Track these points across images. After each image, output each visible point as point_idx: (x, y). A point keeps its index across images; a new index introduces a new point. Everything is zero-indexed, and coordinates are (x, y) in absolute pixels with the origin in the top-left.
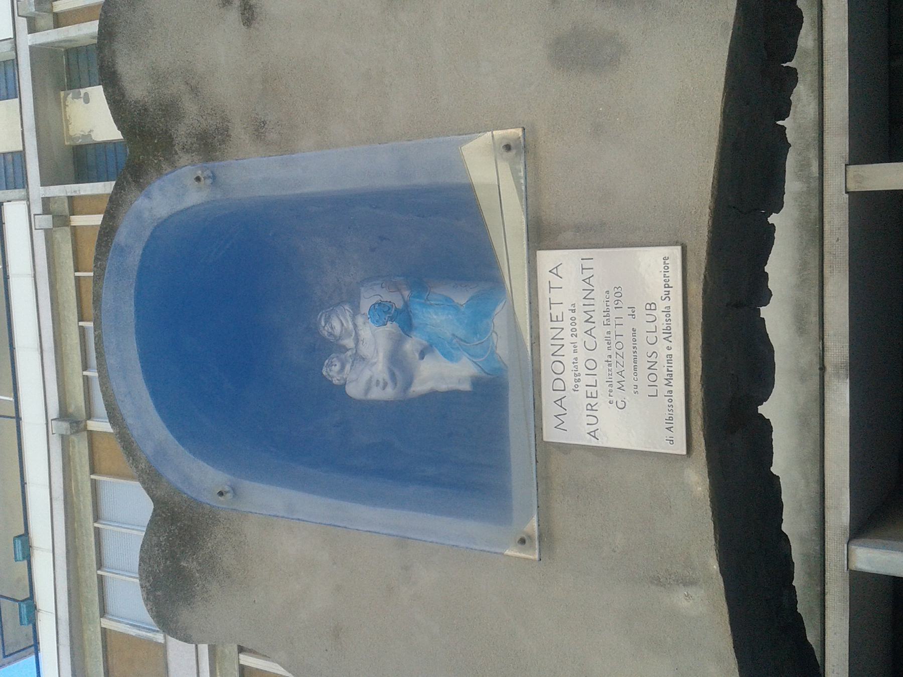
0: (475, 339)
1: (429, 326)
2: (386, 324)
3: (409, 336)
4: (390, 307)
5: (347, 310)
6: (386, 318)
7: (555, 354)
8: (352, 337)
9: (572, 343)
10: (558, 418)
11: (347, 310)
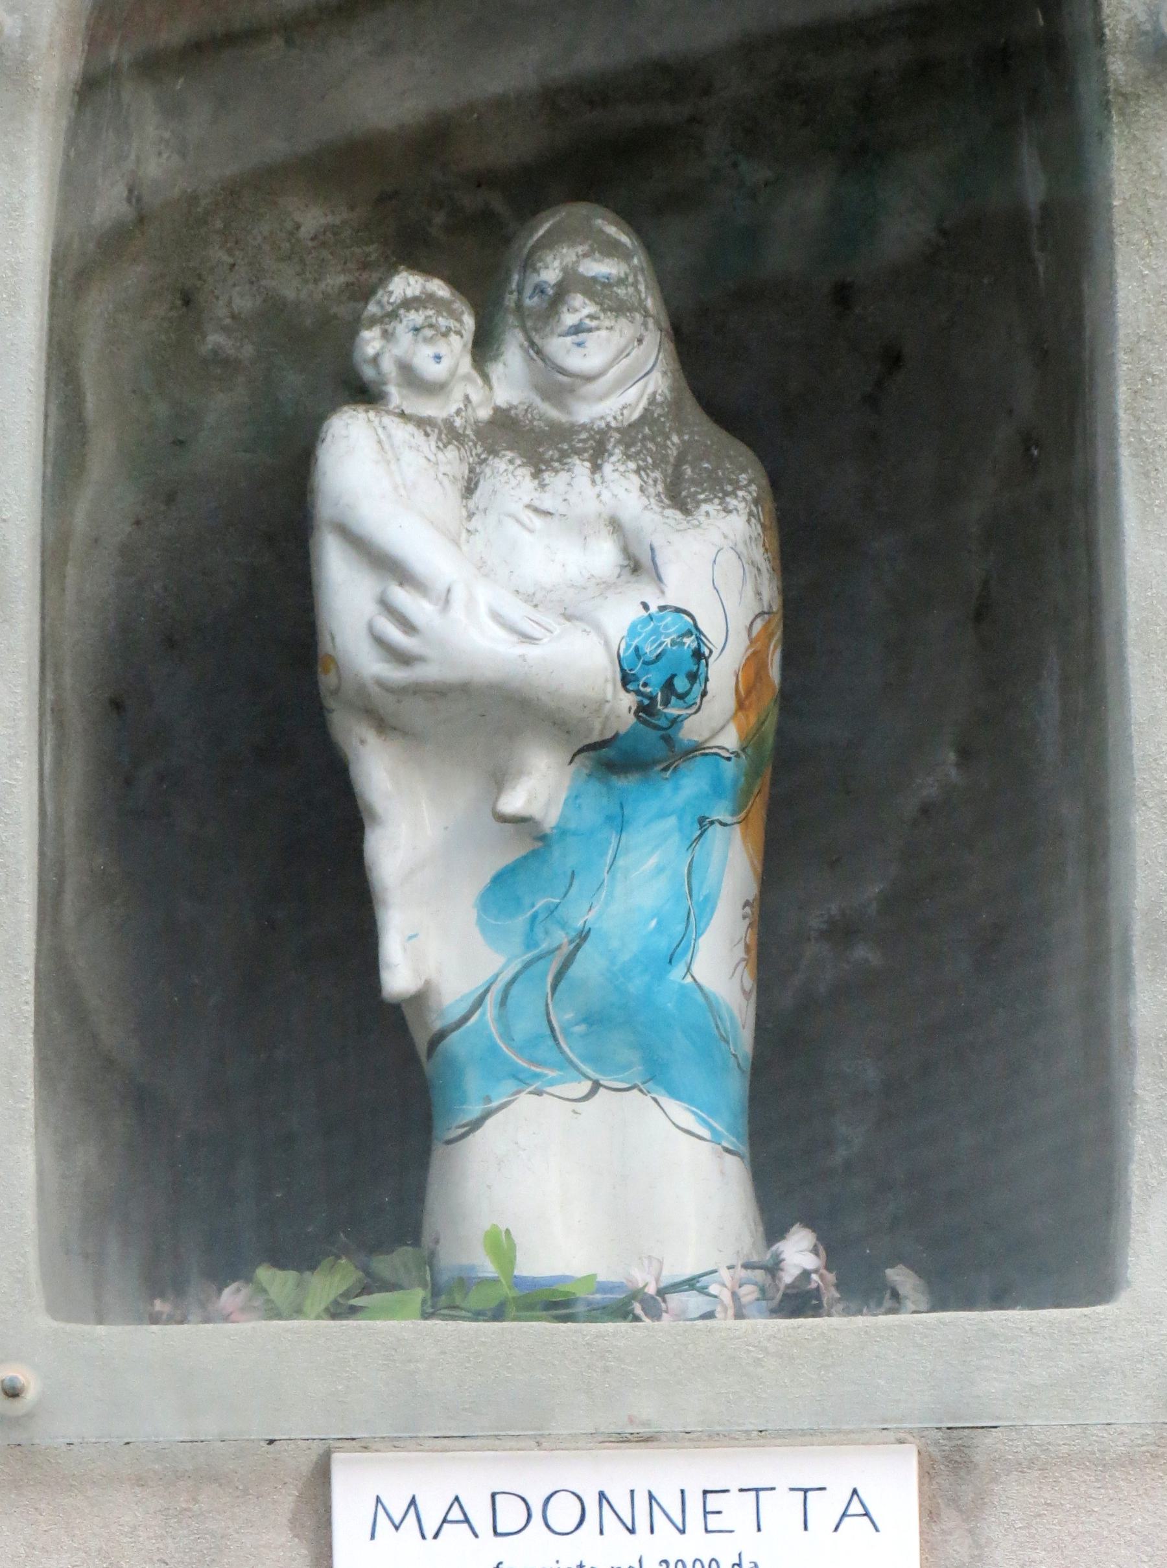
0: (569, 1016)
1: (614, 841)
2: (628, 691)
3: (575, 755)
4: (689, 699)
5: (646, 386)
6: (648, 690)
7: (604, 1502)
8: (537, 401)
9: (640, 1561)
10: (377, 1507)
11: (646, 386)
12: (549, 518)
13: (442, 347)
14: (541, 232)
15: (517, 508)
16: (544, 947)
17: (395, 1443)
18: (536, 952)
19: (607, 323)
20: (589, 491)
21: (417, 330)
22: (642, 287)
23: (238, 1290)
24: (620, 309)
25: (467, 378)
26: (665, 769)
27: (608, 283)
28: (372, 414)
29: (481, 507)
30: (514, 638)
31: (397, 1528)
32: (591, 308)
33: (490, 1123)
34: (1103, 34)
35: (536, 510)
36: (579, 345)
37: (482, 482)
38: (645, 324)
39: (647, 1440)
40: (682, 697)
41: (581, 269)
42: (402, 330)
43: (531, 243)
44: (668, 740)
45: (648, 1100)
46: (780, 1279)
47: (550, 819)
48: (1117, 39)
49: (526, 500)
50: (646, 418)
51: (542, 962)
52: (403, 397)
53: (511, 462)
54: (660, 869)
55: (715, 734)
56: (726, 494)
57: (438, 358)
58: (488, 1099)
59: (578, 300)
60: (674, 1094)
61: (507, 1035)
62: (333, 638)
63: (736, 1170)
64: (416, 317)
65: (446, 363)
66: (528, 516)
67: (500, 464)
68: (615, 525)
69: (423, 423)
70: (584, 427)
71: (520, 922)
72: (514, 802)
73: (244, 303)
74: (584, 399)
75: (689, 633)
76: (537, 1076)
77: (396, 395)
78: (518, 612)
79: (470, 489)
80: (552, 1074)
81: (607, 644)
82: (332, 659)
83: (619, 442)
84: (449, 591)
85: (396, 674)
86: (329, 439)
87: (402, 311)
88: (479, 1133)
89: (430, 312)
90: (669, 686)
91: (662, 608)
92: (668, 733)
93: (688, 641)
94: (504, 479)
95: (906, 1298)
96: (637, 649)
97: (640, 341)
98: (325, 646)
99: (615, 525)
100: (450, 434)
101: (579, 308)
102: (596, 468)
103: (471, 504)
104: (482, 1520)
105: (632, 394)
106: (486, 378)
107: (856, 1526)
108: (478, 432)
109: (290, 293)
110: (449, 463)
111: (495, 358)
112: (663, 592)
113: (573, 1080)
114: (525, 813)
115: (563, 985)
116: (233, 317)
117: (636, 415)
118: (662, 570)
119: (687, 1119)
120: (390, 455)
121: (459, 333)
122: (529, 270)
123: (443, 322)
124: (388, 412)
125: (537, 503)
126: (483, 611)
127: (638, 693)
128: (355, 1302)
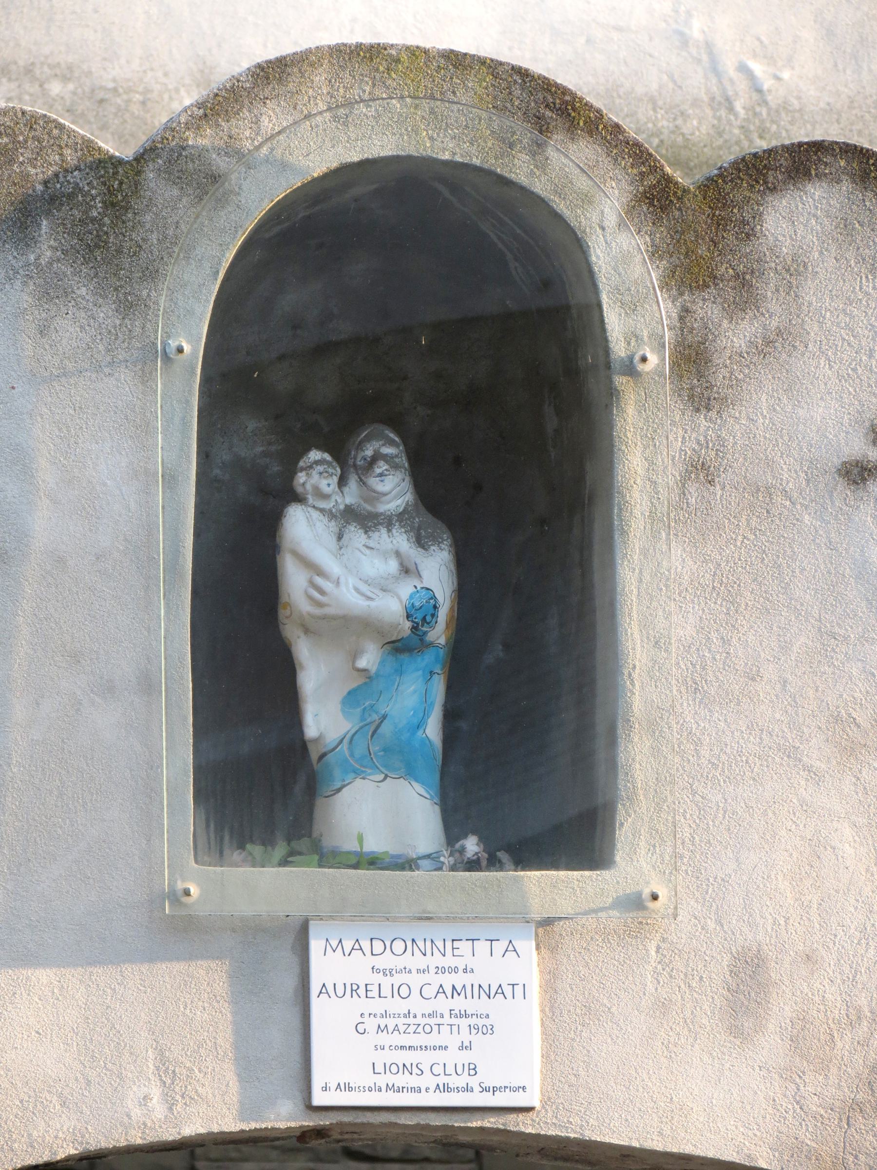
0: (377, 748)
1: (398, 679)
6: (416, 620)
12: (372, 550)
13: (330, 481)
14: (364, 435)
15: (360, 546)
16: (369, 720)
17: (332, 918)
18: (365, 723)
19: (392, 473)
20: (388, 540)
21: (321, 473)
22: (404, 458)
23: (241, 853)
24: (396, 467)
25: (337, 493)
26: (419, 651)
27: (392, 457)
28: (303, 506)
29: (345, 544)
30: (364, 598)
31: (334, 951)
32: (386, 467)
33: (344, 790)
34: (610, 366)
35: (368, 547)
36: (382, 481)
37: (345, 535)
38: (405, 473)
39: (429, 919)
40: (428, 623)
41: (381, 451)
42: (315, 473)
43: (359, 439)
44: (421, 640)
45: (407, 782)
46: (465, 856)
47: (373, 669)
48: (616, 368)
49: (363, 543)
50: (405, 511)
51: (367, 727)
52: (314, 500)
53: (355, 527)
54: (415, 692)
55: (438, 638)
56: (440, 543)
57: (329, 485)
58: (344, 780)
59: (381, 463)
60: (416, 780)
61: (352, 755)
62: (289, 596)
63: (437, 809)
64: (320, 468)
65: (332, 487)
66: (364, 549)
67: (352, 528)
68: (398, 554)
69: (322, 510)
70: (381, 514)
71: (359, 710)
72: (362, 663)
73: (227, 457)
74: (381, 502)
75: (432, 598)
76: (363, 772)
77: (311, 500)
78: (364, 588)
79: (340, 537)
80: (369, 771)
81: (401, 601)
82: (287, 605)
83: (397, 520)
84: (339, 578)
85: (317, 611)
86: (288, 516)
87: (314, 466)
88: (340, 793)
89: (326, 466)
90: (424, 619)
91: (422, 588)
92: (422, 637)
93: (431, 601)
94: (354, 534)
95: (505, 864)
96: (413, 604)
97: (404, 481)
98: (284, 599)
99: (398, 554)
100: (331, 515)
101: (382, 467)
102: (389, 531)
103: (341, 544)
104: (367, 950)
105: (399, 502)
106: (342, 492)
107: (511, 955)
108: (341, 514)
109: (243, 455)
110: (333, 527)
111: (345, 485)
112: (422, 582)
113: (377, 774)
114: (366, 668)
115: (375, 736)
116: (223, 463)
117: (401, 510)
118: (421, 573)
119: (422, 791)
120: (311, 524)
121: (336, 475)
122: (359, 451)
123: (330, 470)
124: (309, 506)
125: (367, 544)
126: (351, 586)
127: (412, 621)
128: (290, 859)
